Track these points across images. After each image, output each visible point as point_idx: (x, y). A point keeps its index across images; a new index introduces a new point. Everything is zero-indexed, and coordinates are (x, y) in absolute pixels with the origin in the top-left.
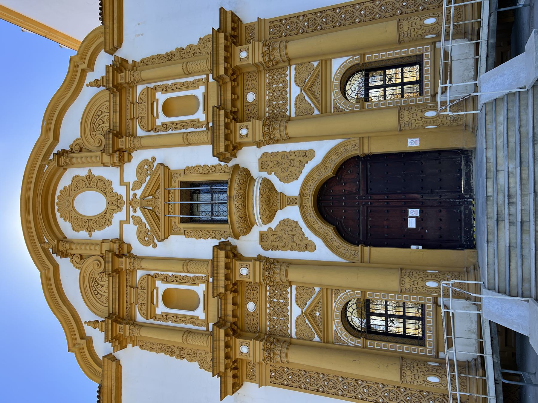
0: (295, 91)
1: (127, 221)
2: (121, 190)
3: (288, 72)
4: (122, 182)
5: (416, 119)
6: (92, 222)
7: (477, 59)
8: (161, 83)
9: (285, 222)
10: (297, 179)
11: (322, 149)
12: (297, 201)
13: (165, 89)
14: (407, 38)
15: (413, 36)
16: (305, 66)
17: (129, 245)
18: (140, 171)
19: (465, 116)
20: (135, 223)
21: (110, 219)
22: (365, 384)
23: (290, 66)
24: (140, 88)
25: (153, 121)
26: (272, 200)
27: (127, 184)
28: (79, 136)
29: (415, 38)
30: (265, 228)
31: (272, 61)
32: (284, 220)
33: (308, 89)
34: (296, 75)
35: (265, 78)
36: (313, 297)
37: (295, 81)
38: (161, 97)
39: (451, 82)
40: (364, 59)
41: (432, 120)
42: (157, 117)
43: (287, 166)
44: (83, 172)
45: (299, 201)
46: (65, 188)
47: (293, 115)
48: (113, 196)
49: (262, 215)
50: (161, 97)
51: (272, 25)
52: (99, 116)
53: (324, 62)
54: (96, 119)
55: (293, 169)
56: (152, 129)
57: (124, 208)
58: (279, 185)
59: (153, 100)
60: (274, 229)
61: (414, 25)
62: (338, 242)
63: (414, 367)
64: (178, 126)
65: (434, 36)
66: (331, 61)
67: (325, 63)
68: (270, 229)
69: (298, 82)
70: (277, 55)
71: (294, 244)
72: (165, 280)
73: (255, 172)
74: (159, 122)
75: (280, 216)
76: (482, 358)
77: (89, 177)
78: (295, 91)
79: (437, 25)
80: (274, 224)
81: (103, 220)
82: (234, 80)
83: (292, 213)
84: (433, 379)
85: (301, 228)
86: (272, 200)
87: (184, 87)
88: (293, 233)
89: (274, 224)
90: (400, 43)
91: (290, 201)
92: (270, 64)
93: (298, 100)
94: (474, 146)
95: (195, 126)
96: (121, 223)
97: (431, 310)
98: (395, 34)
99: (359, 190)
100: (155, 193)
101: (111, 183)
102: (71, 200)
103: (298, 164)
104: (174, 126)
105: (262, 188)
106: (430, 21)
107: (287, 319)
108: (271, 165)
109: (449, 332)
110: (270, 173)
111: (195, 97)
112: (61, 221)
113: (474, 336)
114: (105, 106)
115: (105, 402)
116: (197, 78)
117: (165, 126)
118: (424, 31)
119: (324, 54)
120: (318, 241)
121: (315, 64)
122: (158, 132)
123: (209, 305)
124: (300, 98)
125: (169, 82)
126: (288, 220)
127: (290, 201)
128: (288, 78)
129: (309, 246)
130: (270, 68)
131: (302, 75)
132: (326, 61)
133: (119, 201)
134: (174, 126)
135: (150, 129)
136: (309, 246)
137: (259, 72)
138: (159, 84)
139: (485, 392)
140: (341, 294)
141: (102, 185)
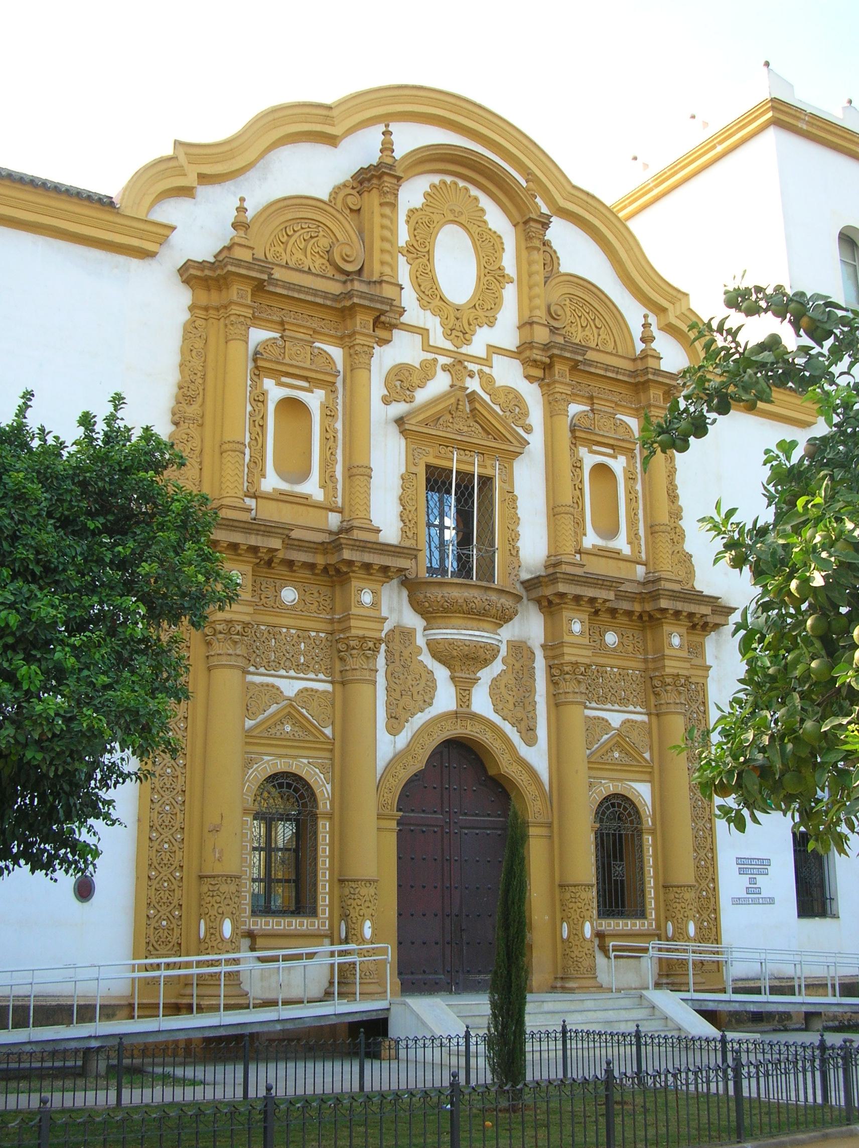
0: (290, 687)
1: (427, 347)
3: (321, 676)
4: (493, 349)
5: (362, 907)
6: (425, 260)
7: (302, 1002)
8: (340, 408)
10: (496, 711)
11: (537, 756)
12: (464, 709)
13: (329, 413)
14: (206, 890)
15: (571, 905)
16: (329, 709)
17: (387, 341)
18: (511, 396)
19: (217, 983)
21: (431, 306)
22: (178, 807)
23: (332, 682)
24: (336, 353)
25: (276, 374)
26: (465, 662)
27: (487, 361)
28: (563, 269)
29: (671, 908)
30: (421, 641)
31: (214, 635)
32: (434, 681)
33: (291, 712)
34: (317, 691)
35: (634, 667)
36: (261, 717)
37: (306, 689)
38: (314, 400)
39: (616, 957)
40: (649, 833)
41: (576, 931)
42: (280, 384)
43: (515, 696)
44: (509, 262)
45: (463, 714)
46: (482, 210)
47: (249, 678)
48: (470, 324)
49: (452, 643)
50: (314, 400)
51: (699, 689)
52: (594, 320)
53: (650, 770)
54: (588, 313)
55: (511, 706)
56: (257, 367)
57: (448, 345)
58: (487, 675)
59: (314, 383)
60: (419, 658)
61: (226, 902)
62: (404, 775)
63: (213, 896)
64: (258, 429)
65: (202, 935)
66: (649, 782)
67: (648, 773)
69: (627, 724)
70: (669, 697)
71: (398, 696)
72: (329, 413)
73: (507, 633)
74: (269, 384)
75: (441, 673)
76: (247, 1007)
77: (500, 277)
78: (290, 687)
79: (219, 940)
80: (426, 658)
81: (430, 294)
82: (640, 617)
83: (445, 699)
85: (422, 710)
86: (465, 662)
87: (328, 454)
88: (416, 696)
90: (341, 881)
91: (464, 697)
92: (342, 646)
93: (275, 691)
94: (535, 990)
95: (252, 465)
96: (423, 332)
98: (219, 870)
99: (466, 814)
100: (476, 422)
101: (491, 324)
102: (462, 219)
103: (519, 715)
104: (258, 418)
105: (479, 646)
106: (692, 929)
107: (273, 666)
108: (518, 666)
110: (504, 661)
111: (304, 475)
113: (626, 986)
114: (607, 338)
115: (3, 182)
116: (340, 486)
117: (261, 399)
118: (680, 921)
119: (661, 771)
120: (403, 739)
121: (328, 731)
122: (252, 380)
123: (316, 510)
124: (275, 693)
125: (339, 425)
126: (435, 688)
127: (464, 697)
128: (631, 708)
130: (334, 642)
131: (315, 704)
132: (331, 751)
133: (461, 335)
134: (258, 418)
135: (260, 363)
136: (395, 723)
137: (332, 621)
138: (340, 401)
139: (228, 1007)
140: (322, 776)
141: (485, 307)
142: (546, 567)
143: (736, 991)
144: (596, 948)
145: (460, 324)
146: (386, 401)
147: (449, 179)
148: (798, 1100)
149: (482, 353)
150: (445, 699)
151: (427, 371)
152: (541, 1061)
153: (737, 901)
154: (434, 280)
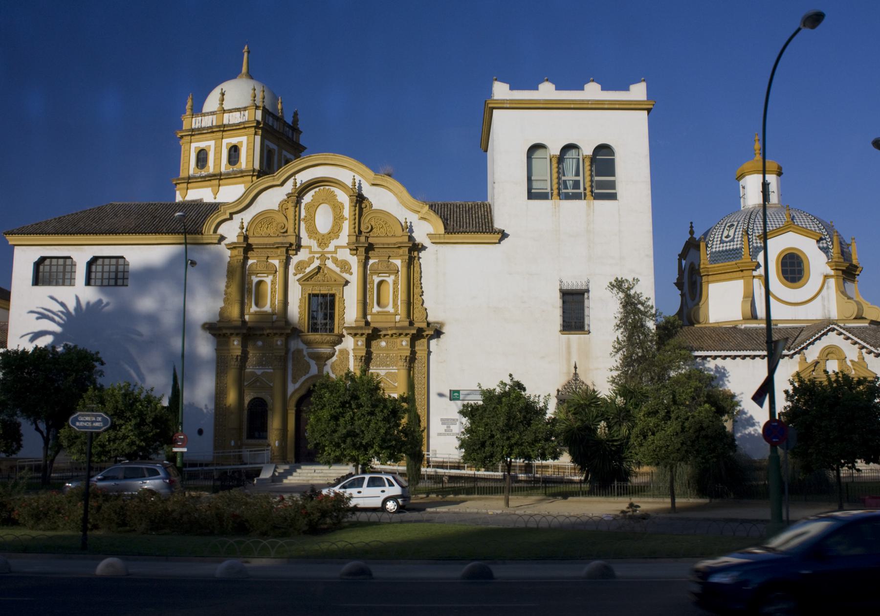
1: (311, 252)
2: (331, 248)
4: (337, 247)
9: (308, 367)
20: (310, 259)
27: (335, 252)
30: (305, 353)
57: (320, 250)
68: (304, 356)
81: (313, 232)
84: (233, 443)
89: (307, 358)
96: (310, 247)
97: (212, 143)
109: (201, 465)
112: (312, 193)
120: (297, 385)
129: (295, 381)
141: (335, 232)
142: (356, 321)
143: (434, 467)
144: (556, 462)
145: (323, 241)
146: (295, 275)
147: (317, 189)
148: (39, 478)
149: (333, 250)
150: (314, 370)
151: (311, 261)
152: (677, 505)
153: (440, 434)
154: (333, 227)
